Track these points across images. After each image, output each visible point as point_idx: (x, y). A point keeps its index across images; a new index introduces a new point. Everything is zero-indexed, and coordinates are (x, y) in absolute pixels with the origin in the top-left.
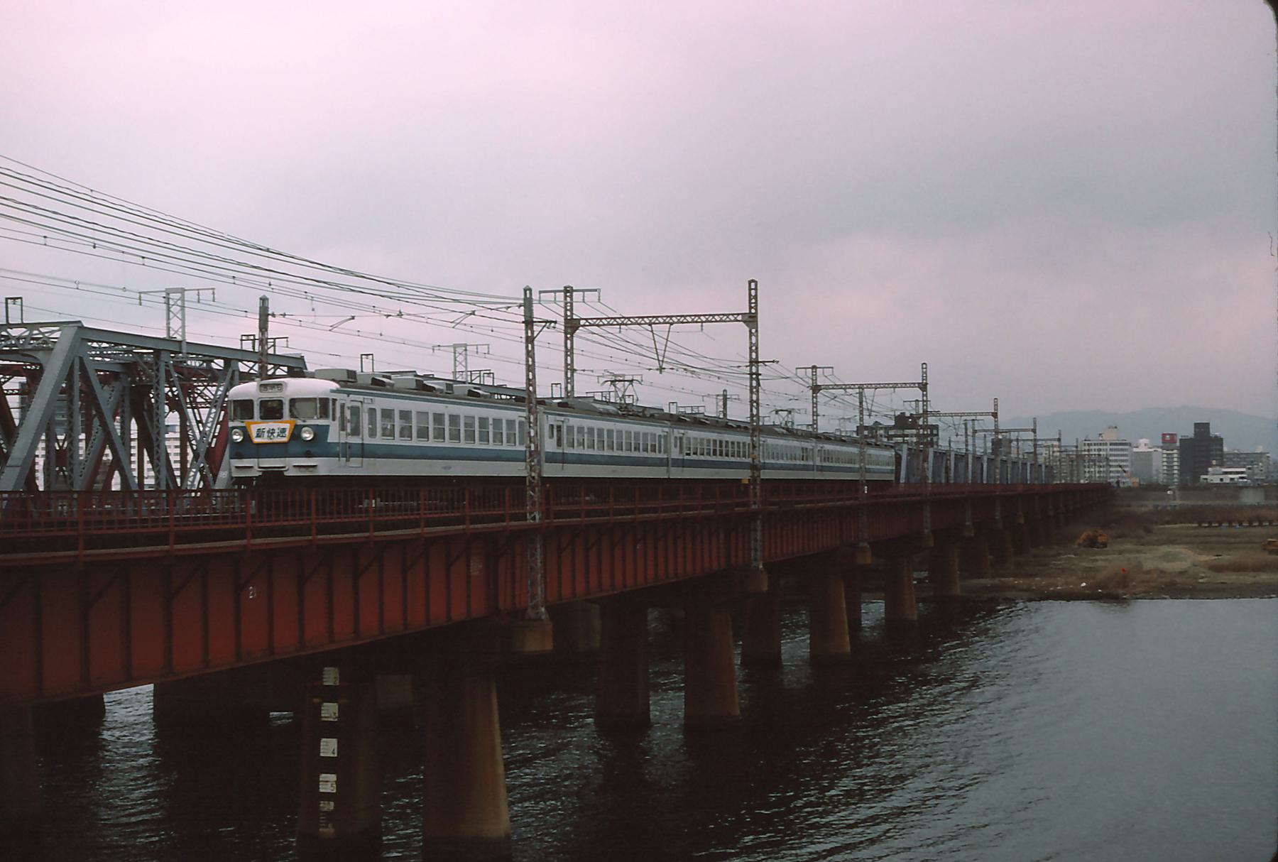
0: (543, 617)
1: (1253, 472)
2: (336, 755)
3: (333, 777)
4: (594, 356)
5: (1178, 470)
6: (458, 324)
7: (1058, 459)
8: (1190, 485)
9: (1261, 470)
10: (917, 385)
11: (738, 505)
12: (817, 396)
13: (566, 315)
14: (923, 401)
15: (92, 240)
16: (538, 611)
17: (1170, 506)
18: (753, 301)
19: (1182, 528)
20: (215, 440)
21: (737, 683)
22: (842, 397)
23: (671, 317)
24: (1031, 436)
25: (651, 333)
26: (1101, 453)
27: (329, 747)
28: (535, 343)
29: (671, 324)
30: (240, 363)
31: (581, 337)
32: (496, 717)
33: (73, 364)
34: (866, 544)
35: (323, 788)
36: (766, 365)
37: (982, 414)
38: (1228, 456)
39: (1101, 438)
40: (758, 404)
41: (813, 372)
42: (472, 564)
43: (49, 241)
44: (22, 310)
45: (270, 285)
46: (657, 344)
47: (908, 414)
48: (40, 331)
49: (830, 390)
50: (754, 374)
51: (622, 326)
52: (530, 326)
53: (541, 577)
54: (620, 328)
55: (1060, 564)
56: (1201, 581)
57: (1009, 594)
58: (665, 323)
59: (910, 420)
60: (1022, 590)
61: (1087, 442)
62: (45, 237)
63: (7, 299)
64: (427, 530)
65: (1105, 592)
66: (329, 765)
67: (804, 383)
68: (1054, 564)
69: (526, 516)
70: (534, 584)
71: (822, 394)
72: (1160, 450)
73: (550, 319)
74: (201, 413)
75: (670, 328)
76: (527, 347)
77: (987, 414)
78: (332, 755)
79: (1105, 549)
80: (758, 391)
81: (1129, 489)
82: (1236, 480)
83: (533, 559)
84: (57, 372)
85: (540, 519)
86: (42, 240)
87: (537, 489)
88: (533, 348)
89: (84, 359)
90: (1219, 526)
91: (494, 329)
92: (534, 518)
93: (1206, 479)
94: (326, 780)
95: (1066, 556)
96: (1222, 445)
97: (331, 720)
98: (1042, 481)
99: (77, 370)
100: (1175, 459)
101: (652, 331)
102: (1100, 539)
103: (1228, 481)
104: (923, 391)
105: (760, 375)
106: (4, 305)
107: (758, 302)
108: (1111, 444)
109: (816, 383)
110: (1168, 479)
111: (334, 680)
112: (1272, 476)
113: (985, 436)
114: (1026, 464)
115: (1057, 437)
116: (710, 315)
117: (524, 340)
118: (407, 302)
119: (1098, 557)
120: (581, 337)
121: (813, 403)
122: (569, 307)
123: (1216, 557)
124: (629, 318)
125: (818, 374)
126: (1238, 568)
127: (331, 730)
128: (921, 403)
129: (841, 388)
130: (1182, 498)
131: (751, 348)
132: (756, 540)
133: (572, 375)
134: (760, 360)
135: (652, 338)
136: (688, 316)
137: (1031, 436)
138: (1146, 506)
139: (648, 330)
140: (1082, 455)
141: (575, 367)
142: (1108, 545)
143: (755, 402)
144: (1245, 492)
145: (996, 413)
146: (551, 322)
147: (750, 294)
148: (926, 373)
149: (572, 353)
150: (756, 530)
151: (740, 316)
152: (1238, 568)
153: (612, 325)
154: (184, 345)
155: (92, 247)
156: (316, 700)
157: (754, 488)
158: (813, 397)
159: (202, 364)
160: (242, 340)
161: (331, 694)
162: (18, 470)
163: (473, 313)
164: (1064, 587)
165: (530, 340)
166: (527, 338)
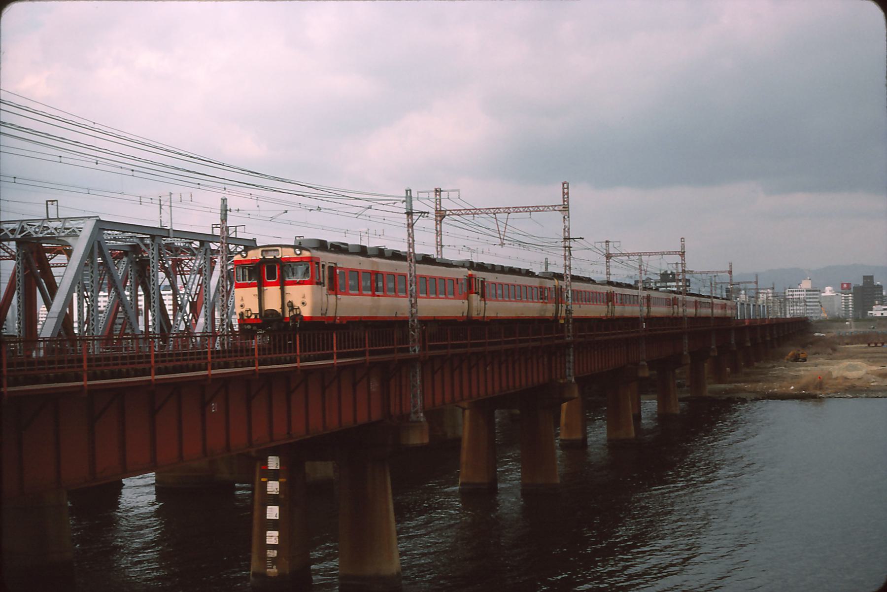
0: (422, 420)
2: (278, 518)
3: (276, 533)
4: (456, 236)
6: (360, 215)
7: (771, 301)
8: (860, 318)
10: (677, 253)
11: (557, 338)
13: (437, 208)
15: (96, 158)
17: (848, 332)
18: (566, 196)
19: (855, 348)
20: (196, 296)
21: (558, 462)
22: (626, 262)
23: (509, 208)
25: (495, 220)
26: (801, 297)
27: (273, 512)
28: (414, 227)
29: (509, 213)
30: (211, 244)
31: (446, 223)
32: (390, 491)
36: (575, 241)
37: (722, 272)
39: (799, 287)
40: (570, 268)
42: (371, 384)
43: (63, 160)
44: (58, 209)
45: (225, 189)
46: (499, 227)
49: (618, 257)
50: (567, 247)
51: (475, 215)
53: (420, 391)
54: (474, 217)
55: (775, 374)
56: (872, 384)
58: (505, 212)
59: (671, 276)
60: (751, 392)
61: (790, 290)
62: (60, 157)
63: (47, 201)
65: (807, 393)
66: (274, 525)
67: (601, 253)
68: (771, 374)
70: (415, 396)
72: (840, 294)
73: (424, 211)
75: (508, 216)
76: (408, 230)
77: (724, 272)
78: (275, 518)
79: (805, 363)
80: (570, 259)
81: (820, 321)
84: (82, 251)
85: (419, 351)
86: (58, 159)
87: (416, 330)
88: (413, 231)
89: (101, 242)
91: (385, 219)
92: (415, 351)
93: (872, 314)
94: (271, 535)
96: (882, 291)
97: (274, 493)
99: (96, 247)
100: (850, 301)
101: (496, 218)
102: (802, 356)
104: (682, 257)
105: (571, 247)
106: (45, 205)
107: (569, 197)
108: (807, 291)
110: (845, 314)
111: (276, 465)
113: (722, 286)
114: (750, 305)
115: (772, 287)
117: (406, 226)
118: (316, 199)
120: (446, 223)
121: (607, 266)
122: (438, 202)
123: (882, 368)
124: (479, 209)
125: (610, 246)
127: (274, 500)
128: (680, 265)
129: (626, 256)
130: (856, 327)
131: (564, 229)
132: (569, 362)
133: (441, 250)
134: (571, 237)
135: (495, 222)
136: (520, 207)
137: (753, 286)
138: (832, 333)
139: (493, 218)
141: (443, 244)
142: (807, 360)
143: (568, 266)
145: (731, 271)
146: (425, 213)
147: (564, 192)
148: (684, 244)
149: (441, 234)
151: (556, 207)
153: (468, 214)
154: (171, 231)
155: (95, 164)
156: (263, 480)
157: (568, 326)
158: (607, 262)
159: (185, 245)
160: (213, 228)
161: (274, 475)
162: (55, 320)
163: (370, 208)
164: (779, 390)
165: (411, 226)
166: (408, 225)
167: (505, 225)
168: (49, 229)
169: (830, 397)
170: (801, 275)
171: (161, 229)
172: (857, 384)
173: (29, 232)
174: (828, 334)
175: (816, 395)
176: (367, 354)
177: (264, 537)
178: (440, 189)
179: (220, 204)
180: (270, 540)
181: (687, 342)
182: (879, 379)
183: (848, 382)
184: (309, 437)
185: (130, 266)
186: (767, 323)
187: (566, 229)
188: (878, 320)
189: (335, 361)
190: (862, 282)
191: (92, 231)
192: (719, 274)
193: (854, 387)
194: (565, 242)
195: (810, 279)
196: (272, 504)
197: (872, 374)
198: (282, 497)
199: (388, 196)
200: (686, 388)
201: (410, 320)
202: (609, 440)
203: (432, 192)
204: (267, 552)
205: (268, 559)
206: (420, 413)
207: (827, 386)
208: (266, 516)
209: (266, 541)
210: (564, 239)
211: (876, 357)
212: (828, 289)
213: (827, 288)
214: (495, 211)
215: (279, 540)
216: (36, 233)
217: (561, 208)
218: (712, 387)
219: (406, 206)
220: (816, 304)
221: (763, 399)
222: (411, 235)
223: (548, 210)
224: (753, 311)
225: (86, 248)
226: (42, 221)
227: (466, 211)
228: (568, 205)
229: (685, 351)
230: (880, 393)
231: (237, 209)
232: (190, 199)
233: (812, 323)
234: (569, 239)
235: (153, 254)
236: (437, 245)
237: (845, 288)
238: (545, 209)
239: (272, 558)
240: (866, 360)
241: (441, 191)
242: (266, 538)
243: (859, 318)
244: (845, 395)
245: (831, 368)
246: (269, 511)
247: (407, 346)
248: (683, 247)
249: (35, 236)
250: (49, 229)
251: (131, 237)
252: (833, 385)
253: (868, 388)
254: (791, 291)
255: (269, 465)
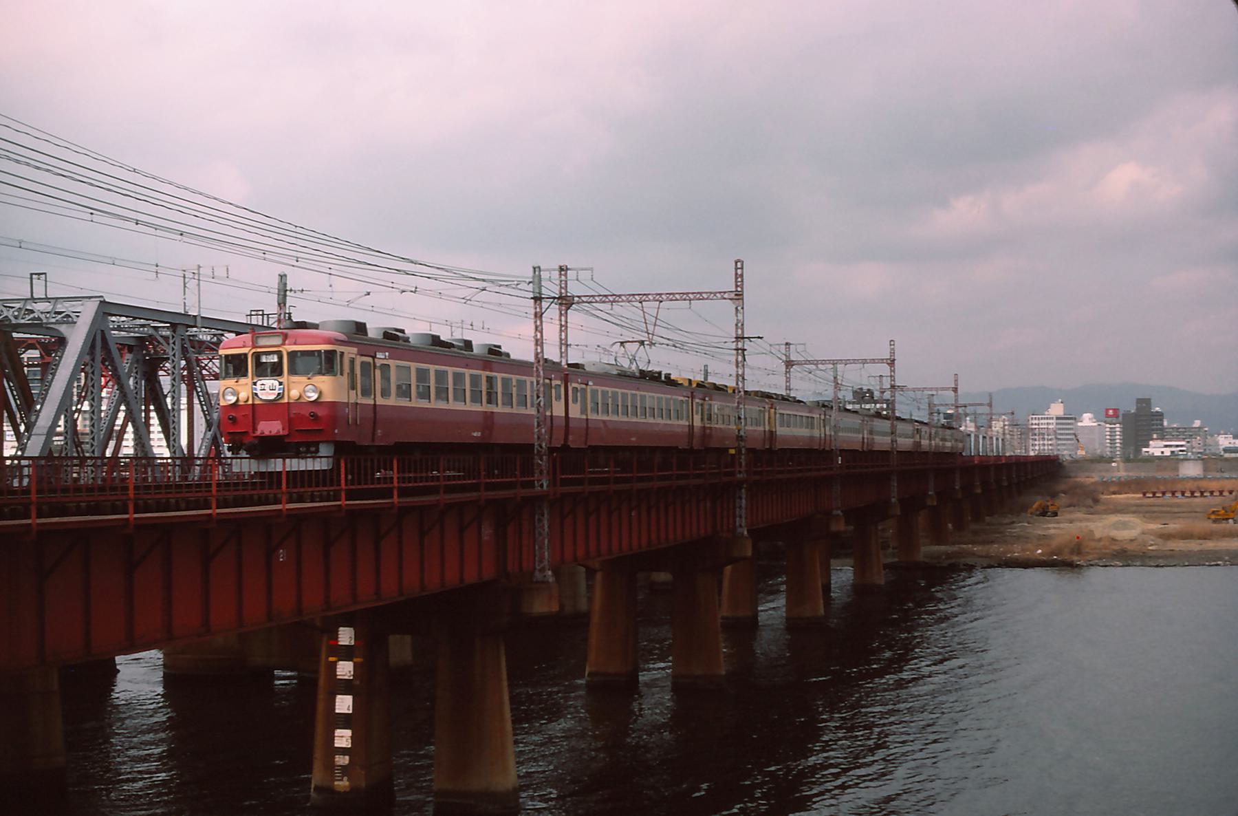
0: (551, 580)
1: (1192, 445)
2: (351, 712)
3: (348, 733)
5: (1120, 443)
8: (1132, 457)
9: (1199, 444)
10: (885, 361)
12: (790, 371)
14: (891, 376)
16: (545, 574)
17: (1115, 477)
18: (739, 280)
24: (986, 409)
25: (642, 312)
26: (1050, 427)
27: (344, 704)
29: (661, 302)
33: (95, 336)
34: (839, 512)
35: (339, 743)
36: (751, 341)
37: (943, 389)
38: (1167, 430)
40: (743, 378)
41: (786, 348)
47: (865, 388)
48: (64, 306)
50: (740, 349)
52: (538, 302)
55: (1015, 532)
56: (1150, 548)
57: (970, 561)
63: (32, 274)
64: (448, 497)
65: (1059, 559)
66: (345, 721)
69: (534, 484)
70: (541, 548)
71: (795, 369)
72: (1102, 424)
74: (207, 384)
76: (536, 322)
77: (947, 389)
78: (347, 712)
79: (1056, 518)
80: (743, 366)
81: (1076, 461)
82: (1176, 453)
83: (541, 525)
84: (81, 344)
85: (547, 486)
87: (544, 457)
89: (106, 332)
90: (1162, 497)
92: (542, 486)
93: (1148, 452)
95: (1020, 524)
97: (346, 677)
98: (971, 452)
103: (1169, 454)
104: (891, 367)
105: (746, 350)
107: (745, 281)
109: (789, 358)
112: (1210, 450)
114: (978, 437)
116: (698, 293)
119: (1050, 526)
125: (791, 349)
126: (1186, 536)
130: (1126, 470)
131: (737, 325)
132: (740, 507)
133: (567, 350)
134: (745, 336)
135: (642, 315)
136: (677, 293)
137: (986, 409)
138: (1092, 478)
140: (1032, 429)
142: (1059, 514)
143: (741, 376)
144: (1186, 464)
145: (956, 388)
147: (736, 274)
148: (893, 349)
150: (741, 498)
151: (726, 294)
152: (1186, 536)
153: (604, 302)
154: (199, 319)
156: (331, 659)
161: (347, 653)
166: (536, 314)
167: (655, 319)
168: (34, 312)
169: (1092, 565)
170: (1049, 397)
171: (186, 315)
172: (1129, 548)
173: (6, 317)
174: (1087, 479)
175: (1073, 561)
176: (395, 493)
177: (332, 738)
178: (567, 266)
179: (277, 281)
180: (339, 741)
181: (896, 485)
182: (1160, 541)
183: (1115, 545)
184: (403, 598)
185: (136, 366)
186: (1004, 462)
187: (740, 325)
188: (1157, 461)
189: (284, 506)
190: (1135, 408)
191: (95, 317)
192: (940, 392)
193: (1125, 551)
194: (738, 342)
195: (1062, 402)
196: (343, 692)
197: (1151, 535)
198: (357, 682)
199: (509, 276)
200: (890, 550)
201: (536, 444)
202: (787, 619)
203: (554, 270)
204: (334, 758)
205: (336, 768)
206: (547, 571)
207: (1087, 550)
208: (335, 709)
209: (334, 743)
210: (736, 338)
211: (1154, 512)
212: (1087, 416)
213: (1085, 415)
214: (641, 298)
215: (352, 743)
216: (16, 317)
217: (733, 295)
218: (928, 550)
219: (534, 288)
220: (1069, 437)
221: (1000, 566)
222: (539, 329)
223: (715, 297)
224: (983, 445)
225: (85, 340)
226: (24, 301)
227: (601, 297)
228: (742, 291)
229: (894, 497)
230: (1160, 560)
231: (301, 289)
232: (226, 275)
233: (1065, 463)
234: (743, 338)
235: (173, 349)
236: (561, 344)
237: (1112, 415)
238: (711, 297)
239: (340, 766)
240: (1141, 515)
241: (567, 269)
242: (334, 740)
243: (1129, 457)
244: (1113, 562)
245: (1092, 526)
246: (339, 705)
247: (733, 469)
248: (893, 353)
249: (14, 321)
250: (34, 312)
251: (143, 326)
252: (1095, 549)
253: (1144, 553)
254: (1035, 418)
255: (339, 639)
